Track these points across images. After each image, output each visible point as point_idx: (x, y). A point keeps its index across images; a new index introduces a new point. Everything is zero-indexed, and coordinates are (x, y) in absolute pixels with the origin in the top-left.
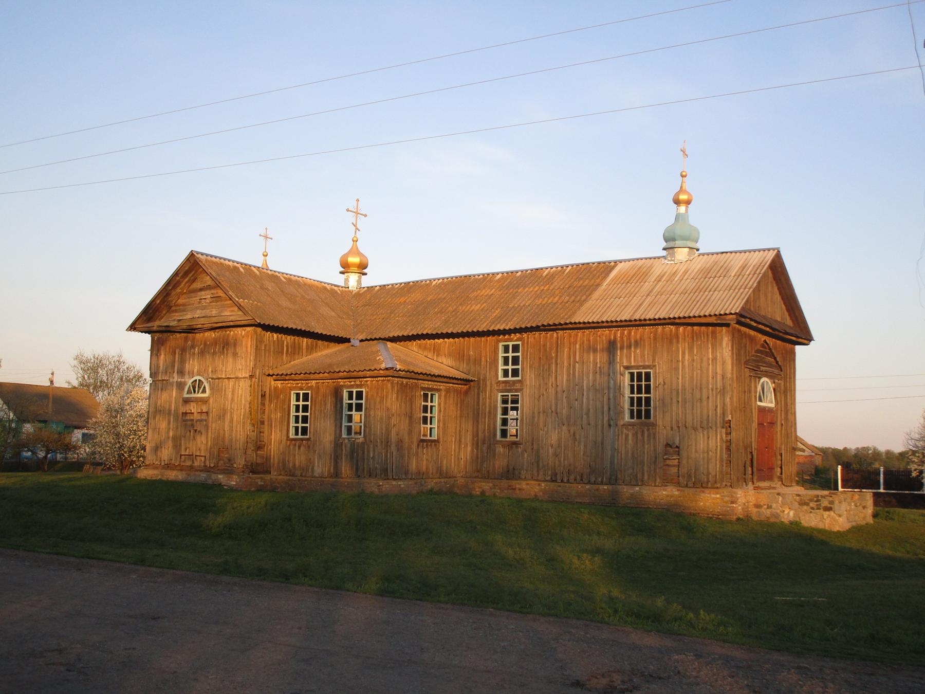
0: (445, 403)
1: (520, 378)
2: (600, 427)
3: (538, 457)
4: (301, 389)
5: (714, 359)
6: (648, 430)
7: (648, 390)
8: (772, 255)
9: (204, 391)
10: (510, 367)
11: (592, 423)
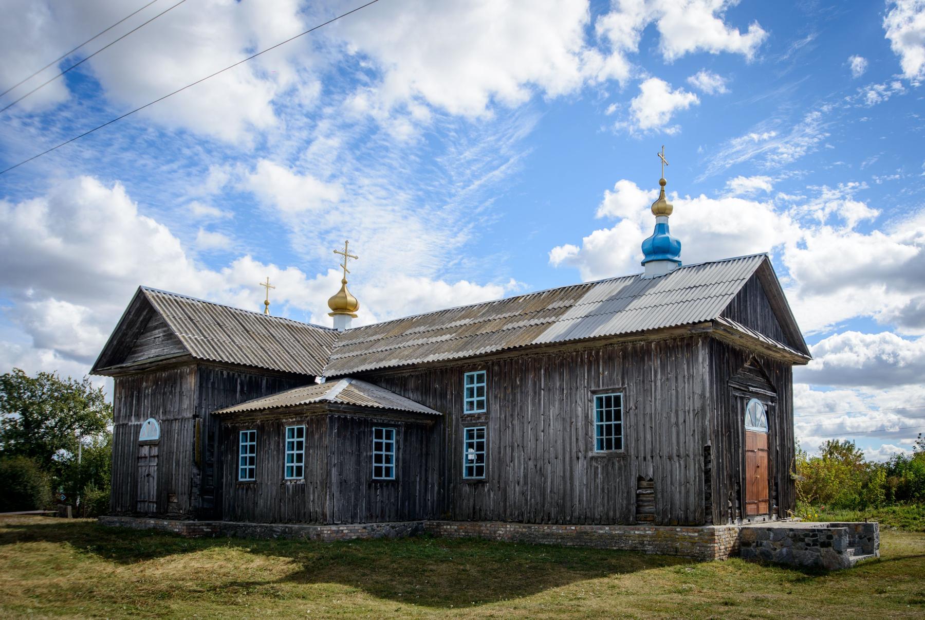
0: (405, 440)
1: (485, 411)
2: (567, 459)
4: (248, 429)
5: (691, 377)
6: (619, 462)
7: (618, 417)
8: (757, 263)
10: (475, 399)
11: (560, 457)
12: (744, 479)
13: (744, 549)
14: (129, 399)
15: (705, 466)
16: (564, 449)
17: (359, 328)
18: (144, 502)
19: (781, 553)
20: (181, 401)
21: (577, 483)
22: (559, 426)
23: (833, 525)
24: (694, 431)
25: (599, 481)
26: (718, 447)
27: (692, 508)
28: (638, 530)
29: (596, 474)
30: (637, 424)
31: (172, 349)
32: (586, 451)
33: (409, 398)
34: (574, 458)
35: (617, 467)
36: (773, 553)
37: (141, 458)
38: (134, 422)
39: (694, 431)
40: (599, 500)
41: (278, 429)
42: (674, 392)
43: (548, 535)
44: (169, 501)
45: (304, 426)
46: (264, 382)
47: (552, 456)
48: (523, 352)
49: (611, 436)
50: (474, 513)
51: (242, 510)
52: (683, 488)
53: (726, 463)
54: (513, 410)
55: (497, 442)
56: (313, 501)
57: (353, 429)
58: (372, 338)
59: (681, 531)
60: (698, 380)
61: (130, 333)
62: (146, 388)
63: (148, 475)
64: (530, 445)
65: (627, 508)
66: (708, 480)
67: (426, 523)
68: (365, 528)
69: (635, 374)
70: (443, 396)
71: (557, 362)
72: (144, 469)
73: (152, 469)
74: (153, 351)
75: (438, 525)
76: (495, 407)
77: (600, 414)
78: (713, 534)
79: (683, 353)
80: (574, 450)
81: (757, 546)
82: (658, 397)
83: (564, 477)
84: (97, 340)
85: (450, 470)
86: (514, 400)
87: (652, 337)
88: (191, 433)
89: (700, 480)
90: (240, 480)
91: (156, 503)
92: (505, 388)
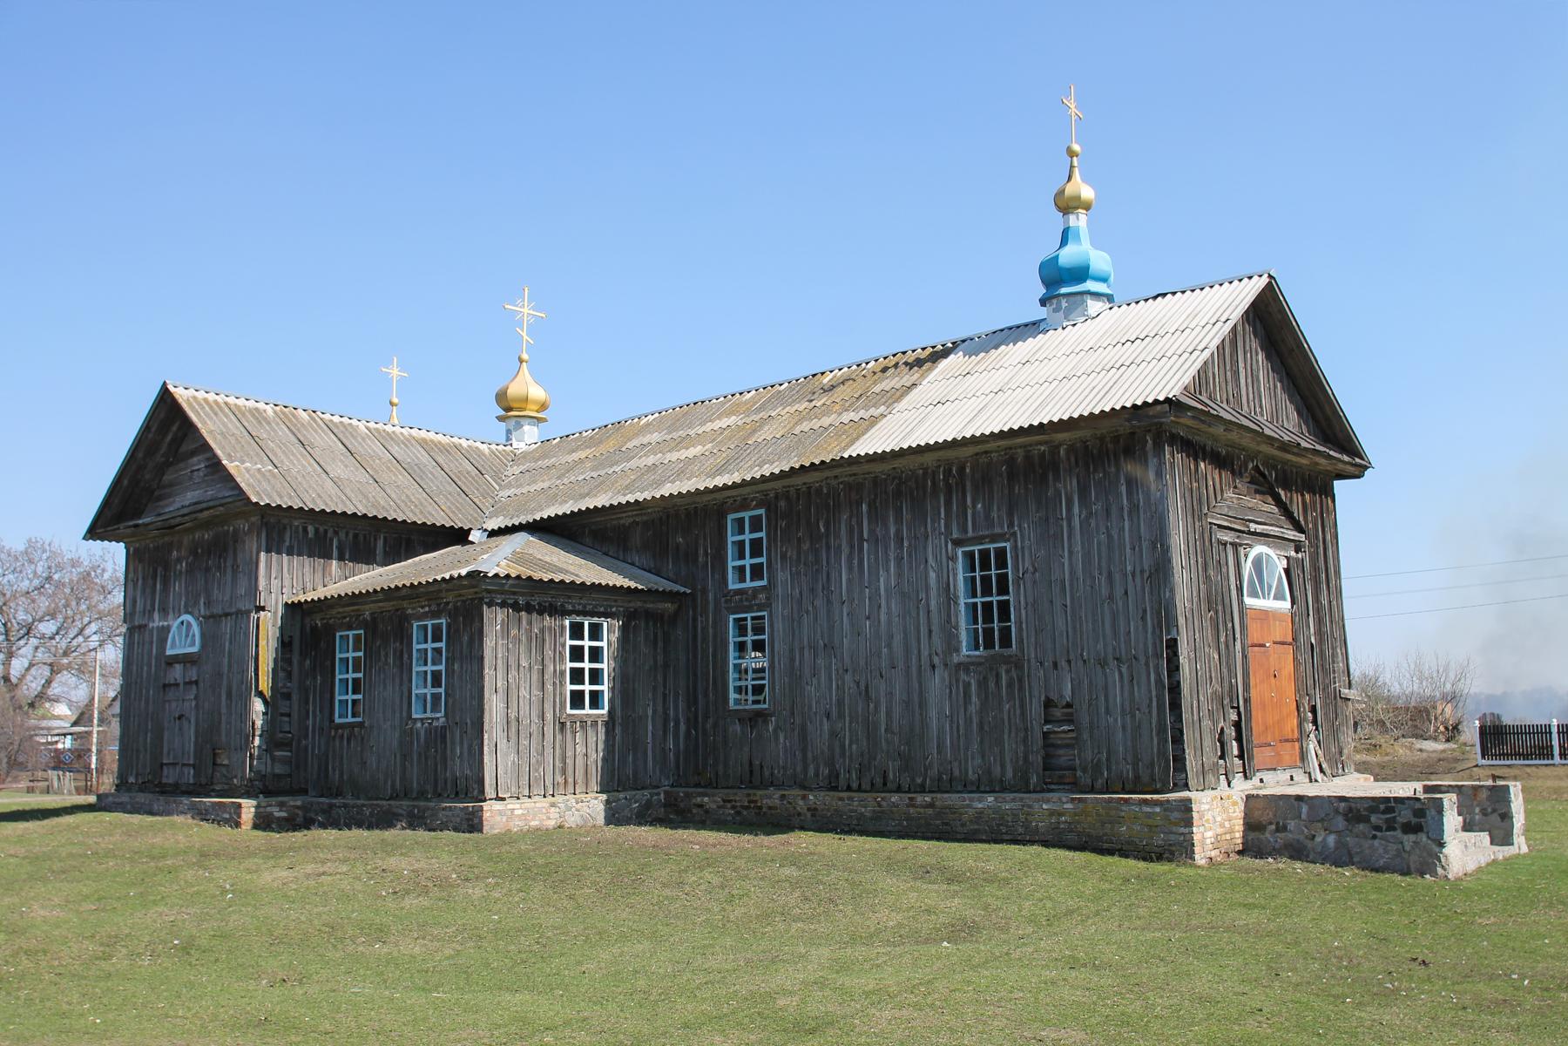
1: (764, 583)
4: (350, 628)
6: (1008, 672)
7: (1003, 589)
9: (193, 644)
11: (901, 665)
14: (150, 582)
28: (1048, 801)
36: (1309, 844)
38: (157, 622)
49: (993, 621)
65: (1026, 758)
72: (174, 705)
80: (925, 653)
81: (1277, 830)
92: (799, 539)
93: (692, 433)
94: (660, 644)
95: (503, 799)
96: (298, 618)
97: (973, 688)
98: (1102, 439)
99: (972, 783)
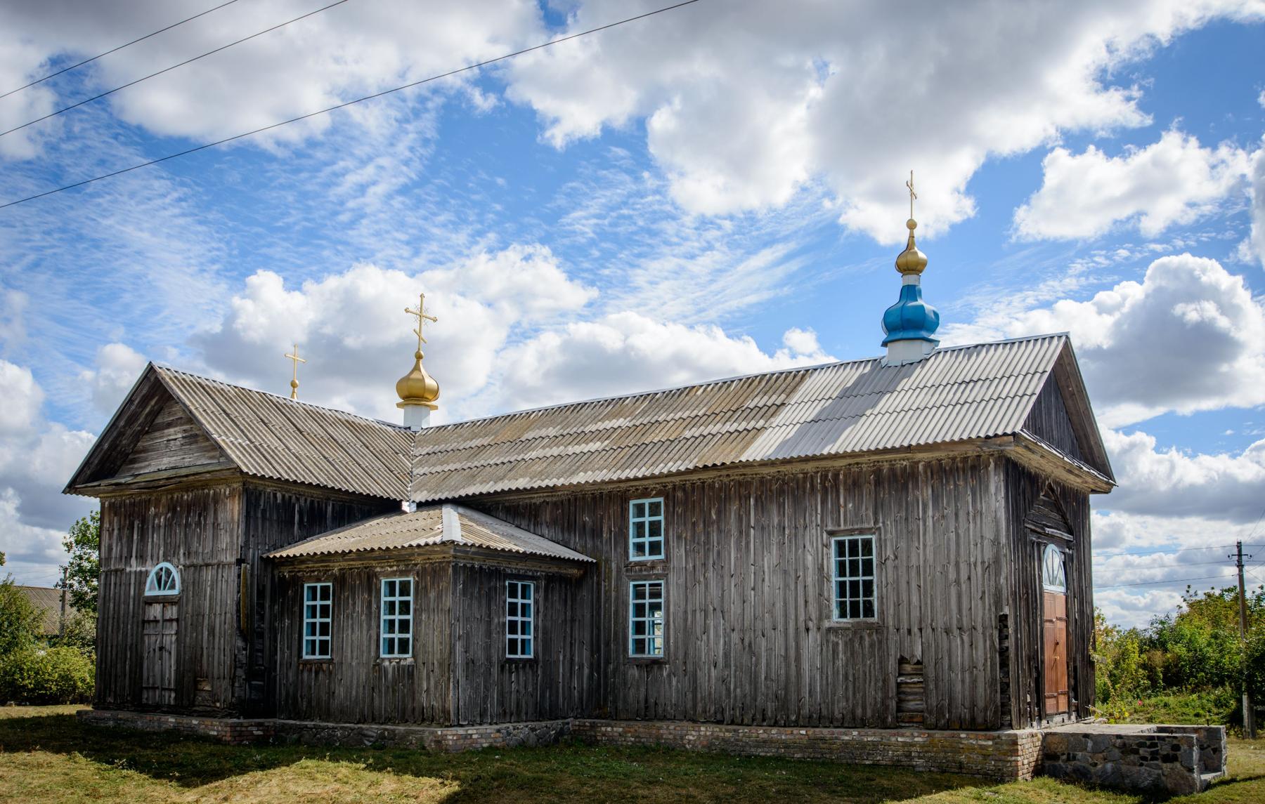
0: (546, 598)
1: (662, 557)
3: (695, 681)
4: (319, 580)
6: (870, 635)
7: (868, 570)
8: (1056, 348)
9: (173, 587)
10: (647, 540)
11: (780, 627)
12: (1043, 662)
13: (1056, 763)
14: (126, 531)
15: (1000, 643)
16: (786, 616)
17: (445, 427)
18: (154, 688)
19: (1104, 771)
20: (215, 537)
21: (806, 666)
22: (778, 581)
23: (1160, 730)
24: (984, 592)
25: (840, 663)
26: (1016, 616)
27: (981, 704)
28: (903, 736)
29: (835, 652)
30: (897, 581)
31: (198, 458)
32: (820, 619)
33: (543, 536)
34: (802, 628)
35: (867, 643)
36: (1093, 770)
37: (149, 622)
38: (134, 567)
39: (984, 592)
40: (840, 692)
41: (369, 581)
42: (953, 536)
43: (765, 741)
44: (196, 689)
45: (411, 579)
46: (330, 509)
47: (768, 625)
48: (724, 473)
49: (856, 598)
50: (646, 708)
51: (310, 702)
52: (967, 675)
53: (1025, 641)
54: (706, 557)
55: (682, 604)
56: (428, 690)
57: (481, 583)
58: (474, 443)
59: (967, 738)
60: (988, 520)
61: (129, 432)
62: (156, 515)
63: (161, 649)
64: (734, 609)
65: (883, 703)
66: (1004, 664)
67: (573, 723)
68: (498, 731)
69: (894, 508)
70: (596, 533)
71: (774, 487)
72: (153, 638)
73: (167, 640)
74: (166, 458)
75: (593, 726)
76: (679, 553)
77: (841, 565)
78: (1015, 743)
79: (965, 480)
80: (802, 618)
81: (1068, 759)
82: (930, 542)
83: (786, 657)
84: (78, 444)
85: (608, 644)
86: (707, 542)
87: (919, 456)
88: (233, 586)
89: (993, 665)
90: (305, 657)
91: (175, 691)
92: (694, 524)
93: (587, 430)
94: (569, 603)
95: (462, 726)
96: (269, 570)
97: (841, 648)
98: (954, 459)
99: (837, 720)
